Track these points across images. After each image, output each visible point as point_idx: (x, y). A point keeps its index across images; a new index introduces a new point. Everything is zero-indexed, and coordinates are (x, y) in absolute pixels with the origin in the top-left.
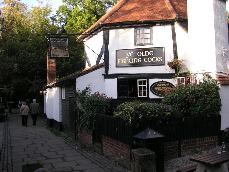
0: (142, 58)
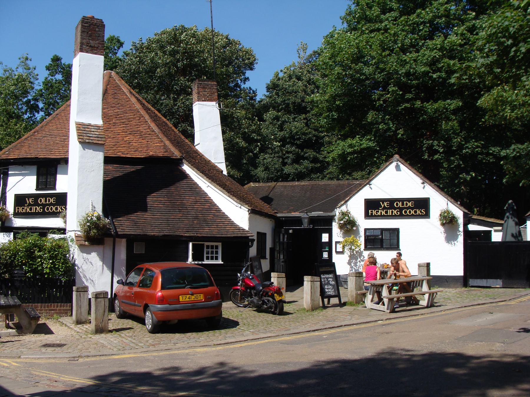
0: (44, 206)
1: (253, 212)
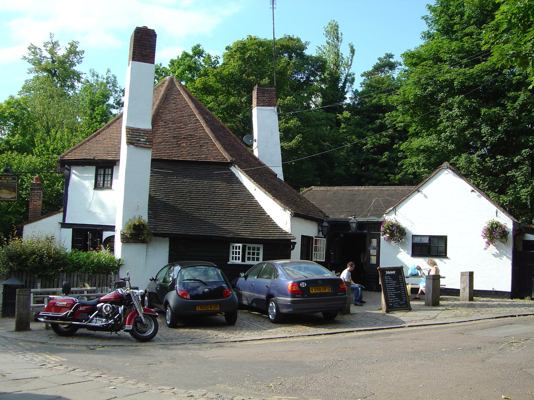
1: (295, 215)
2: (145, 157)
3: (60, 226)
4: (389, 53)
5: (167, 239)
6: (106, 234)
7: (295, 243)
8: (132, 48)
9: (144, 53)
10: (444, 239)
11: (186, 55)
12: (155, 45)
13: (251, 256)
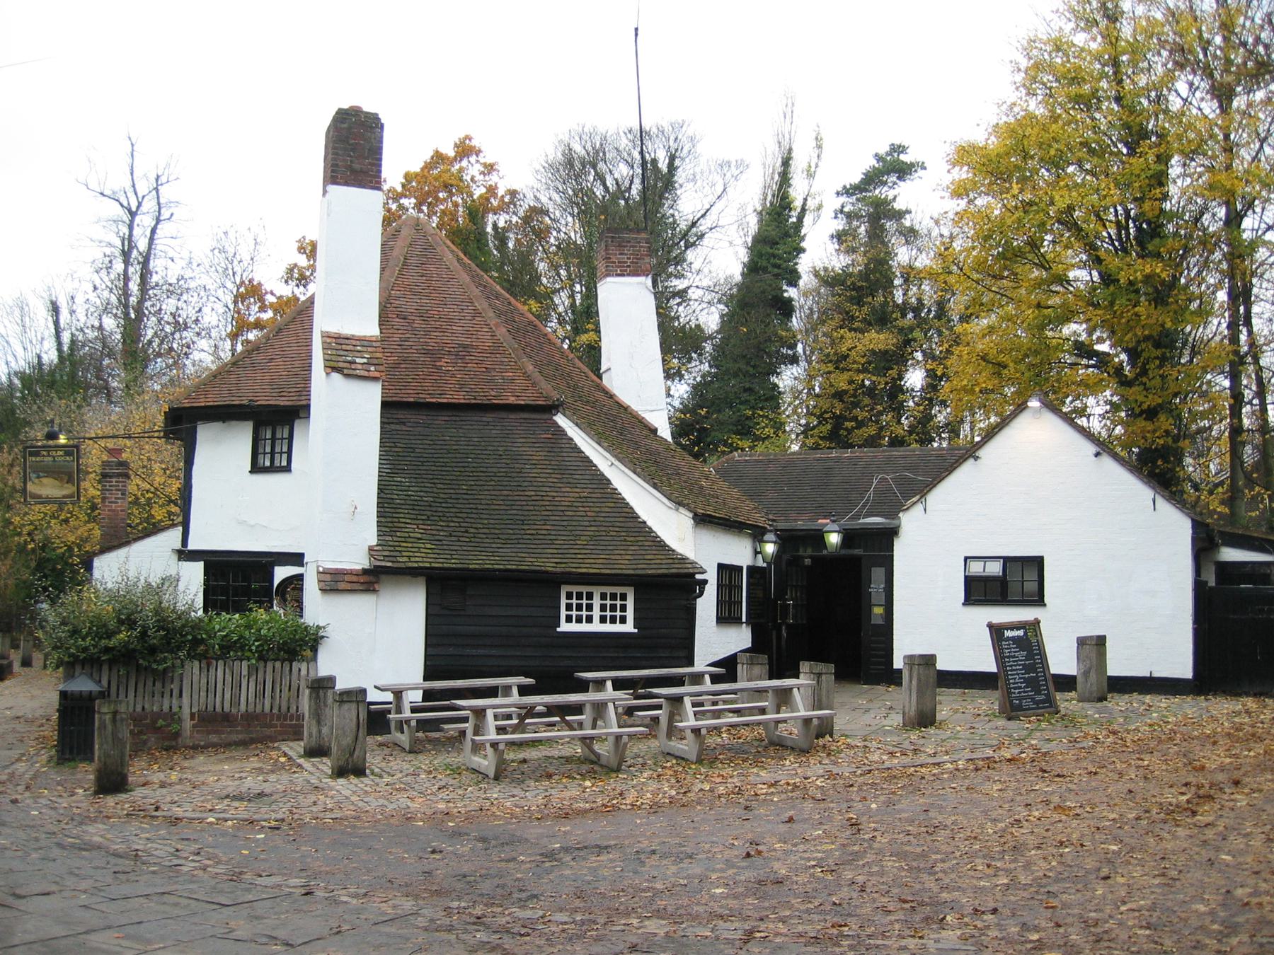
2: (370, 397)
3: (175, 557)
4: (897, 142)
5: (422, 580)
6: (281, 573)
7: (705, 582)
8: (330, 156)
9: (357, 166)
10: (1037, 563)
11: (438, 158)
12: (381, 148)
13: (608, 613)
